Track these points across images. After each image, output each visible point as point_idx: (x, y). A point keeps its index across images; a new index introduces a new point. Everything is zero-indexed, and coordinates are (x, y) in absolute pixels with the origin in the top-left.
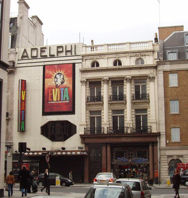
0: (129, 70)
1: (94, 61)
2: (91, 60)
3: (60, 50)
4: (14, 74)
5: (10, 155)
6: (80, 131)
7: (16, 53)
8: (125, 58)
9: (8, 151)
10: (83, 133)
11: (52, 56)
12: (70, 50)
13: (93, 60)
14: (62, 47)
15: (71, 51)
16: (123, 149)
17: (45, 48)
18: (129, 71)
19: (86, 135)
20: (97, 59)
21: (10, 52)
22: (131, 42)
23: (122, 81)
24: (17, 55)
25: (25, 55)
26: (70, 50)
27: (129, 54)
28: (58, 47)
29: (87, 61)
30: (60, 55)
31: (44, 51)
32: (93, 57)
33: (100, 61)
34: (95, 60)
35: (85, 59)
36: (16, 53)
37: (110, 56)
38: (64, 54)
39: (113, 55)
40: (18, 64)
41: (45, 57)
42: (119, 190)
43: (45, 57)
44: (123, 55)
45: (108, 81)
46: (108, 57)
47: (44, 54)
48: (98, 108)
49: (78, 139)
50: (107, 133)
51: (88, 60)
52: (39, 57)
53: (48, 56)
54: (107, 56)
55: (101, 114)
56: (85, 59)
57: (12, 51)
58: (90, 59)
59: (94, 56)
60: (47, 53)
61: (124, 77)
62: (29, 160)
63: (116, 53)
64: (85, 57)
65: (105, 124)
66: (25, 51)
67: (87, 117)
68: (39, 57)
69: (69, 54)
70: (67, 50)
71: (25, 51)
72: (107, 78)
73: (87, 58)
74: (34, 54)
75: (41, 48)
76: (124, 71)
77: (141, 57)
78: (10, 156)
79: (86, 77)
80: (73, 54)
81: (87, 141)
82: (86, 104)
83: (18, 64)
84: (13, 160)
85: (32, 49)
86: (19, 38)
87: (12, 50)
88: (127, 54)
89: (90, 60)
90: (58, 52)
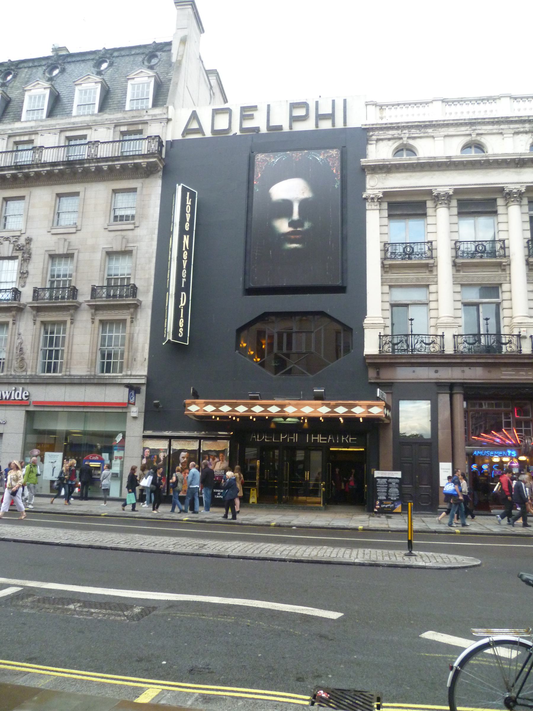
0: (517, 167)
1: (403, 143)
2: (394, 141)
3: (300, 112)
5: (135, 415)
7: (169, 120)
8: (499, 137)
9: (132, 401)
12: (330, 112)
13: (401, 142)
14: (304, 105)
16: (497, 405)
17: (255, 108)
18: (518, 170)
19: (386, 357)
20: (414, 138)
21: (150, 118)
22: (515, 93)
23: (423, 205)
24: (171, 124)
26: (330, 112)
27: (512, 126)
28: (294, 106)
29: (381, 144)
31: (251, 117)
32: (399, 132)
33: (485, 140)
34: (405, 140)
35: (374, 137)
36: (169, 120)
37: (452, 131)
39: (463, 128)
42: (243, 520)
44: (490, 127)
45: (380, 200)
46: (446, 133)
48: (418, 278)
49: (489, 372)
50: (455, 350)
51: (385, 142)
54: (444, 131)
55: (498, 297)
56: (374, 137)
57: (155, 115)
58: (389, 139)
59: (404, 132)
61: (430, 192)
62: (199, 430)
63: (472, 123)
64: (376, 133)
65: (374, 326)
66: (194, 116)
67: (509, 306)
70: (321, 112)
71: (194, 116)
72: (446, 189)
73: (381, 134)
75: (243, 109)
76: (501, 170)
77: (411, 142)
78: (135, 418)
79: (380, 185)
82: (383, 266)
84: (145, 428)
85: (216, 112)
86: (177, 84)
87: (157, 111)
88: (502, 127)
89: (391, 143)
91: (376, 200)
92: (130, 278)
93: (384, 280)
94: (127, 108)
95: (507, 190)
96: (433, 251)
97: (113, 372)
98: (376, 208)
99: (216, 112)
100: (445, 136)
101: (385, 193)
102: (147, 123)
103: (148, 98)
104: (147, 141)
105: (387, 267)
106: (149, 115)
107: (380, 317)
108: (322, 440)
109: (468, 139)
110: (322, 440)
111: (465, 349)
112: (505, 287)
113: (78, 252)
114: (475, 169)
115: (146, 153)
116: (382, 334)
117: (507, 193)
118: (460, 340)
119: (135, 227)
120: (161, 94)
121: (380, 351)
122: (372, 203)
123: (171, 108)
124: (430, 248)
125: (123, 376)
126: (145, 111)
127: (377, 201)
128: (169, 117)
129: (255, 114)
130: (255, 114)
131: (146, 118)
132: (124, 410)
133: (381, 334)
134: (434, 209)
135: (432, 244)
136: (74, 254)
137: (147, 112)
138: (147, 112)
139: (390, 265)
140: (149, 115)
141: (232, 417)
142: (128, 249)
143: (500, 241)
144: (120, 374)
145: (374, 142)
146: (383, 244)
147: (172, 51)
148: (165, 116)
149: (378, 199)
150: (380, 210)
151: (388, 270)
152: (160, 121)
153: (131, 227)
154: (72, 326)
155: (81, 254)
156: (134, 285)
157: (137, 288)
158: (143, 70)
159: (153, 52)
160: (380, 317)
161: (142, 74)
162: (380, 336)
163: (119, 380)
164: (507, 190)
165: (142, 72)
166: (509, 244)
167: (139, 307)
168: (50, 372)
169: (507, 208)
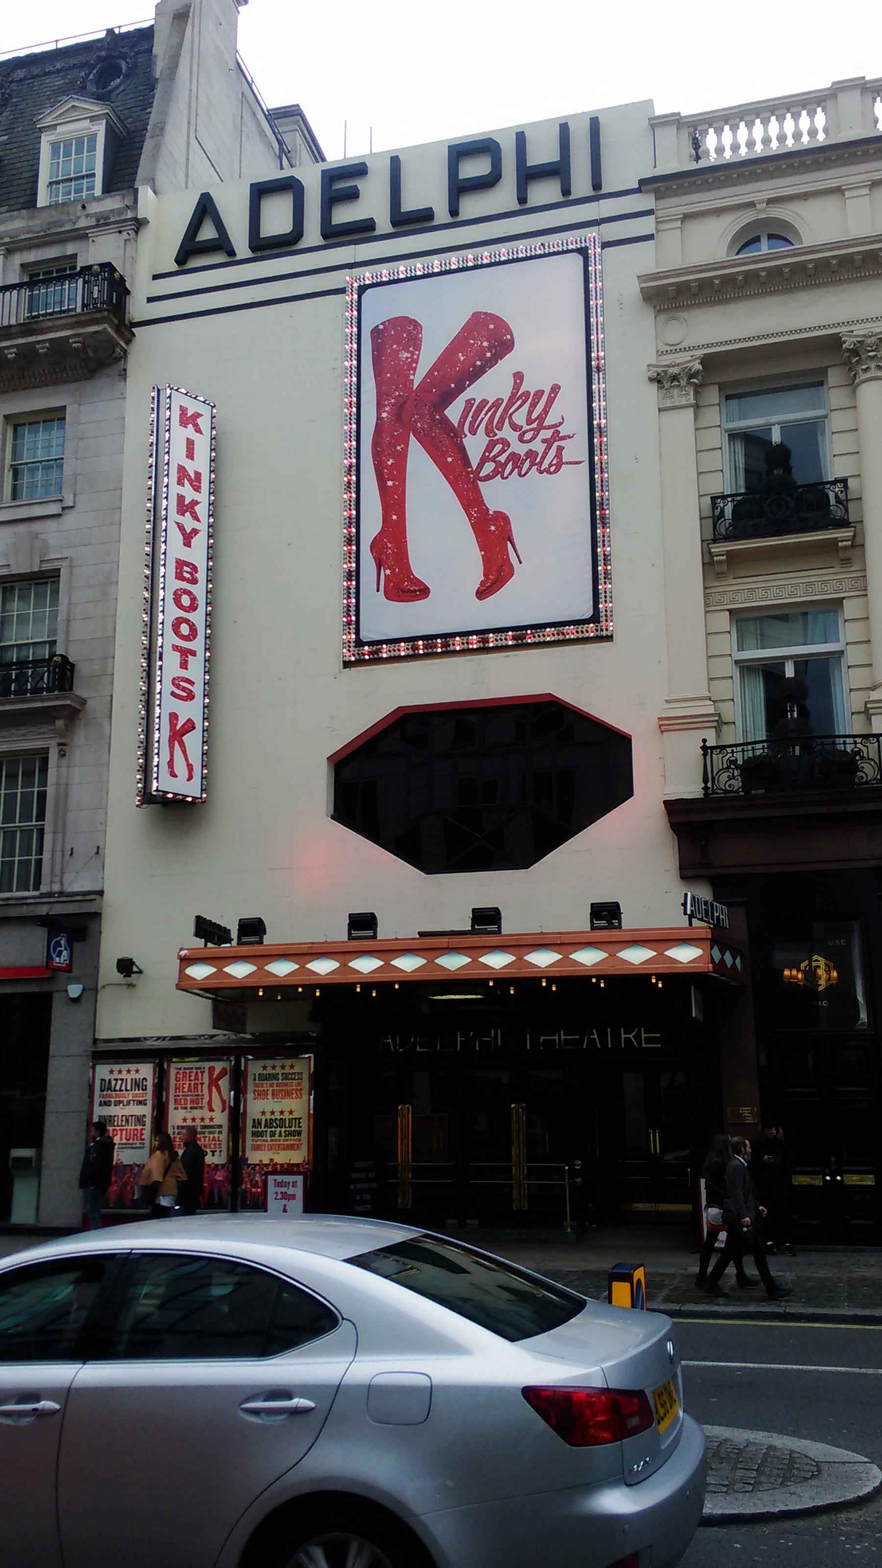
3: (475, 168)
4: (123, 375)
6: (666, 770)
7: (139, 224)
10: (690, 788)
11: (422, 220)
14: (485, 147)
15: (558, 171)
24: (147, 236)
25: (207, 233)
28: (460, 152)
30: (472, 206)
31: (353, 195)
38: (504, 196)
40: (150, 300)
41: (363, 230)
43: (363, 230)
46: (773, 194)
47: (343, 215)
52: (312, 235)
53: (384, 225)
60: (372, 204)
66: (206, 208)
68: (312, 235)
69: (544, 192)
71: (206, 208)
74: (277, 218)
80: (581, 185)
81: (737, 854)
83: (150, 300)
86: (162, 129)
87: (113, 203)
90: (459, 189)
91: (683, 383)
92: (55, 641)
93: (860, 583)
94: (42, 200)
95: (849, 343)
96: (851, 505)
97: (17, 891)
98: (684, 402)
99: (260, 192)
100: (687, 217)
101: (706, 361)
102: (85, 237)
103: (93, 175)
104: (81, 281)
105: (720, 562)
106: (87, 216)
107: (704, 698)
108: (648, 1041)
109: (748, 217)
110: (648, 1041)
111: (732, 782)
112: (851, 608)
113: (71, 567)
114: (817, 286)
115: (22, 321)
116: (711, 743)
117: (854, 352)
118: (717, 759)
119: (63, 508)
120: (124, 161)
121: (705, 789)
122: (676, 392)
123: (145, 194)
124: (842, 496)
125: (42, 896)
126: (79, 207)
127: (689, 383)
128: (140, 216)
129: (361, 184)
130: (361, 184)
131: (83, 223)
132: (46, 988)
133: (707, 744)
134: (849, 389)
135: (846, 487)
136: (59, 570)
137: (84, 207)
138: (84, 207)
139: (729, 554)
140: (87, 216)
141: (598, 982)
142: (46, 567)
143: (834, 482)
144: (36, 893)
145: (679, 224)
146: (708, 501)
147: (155, 50)
148: (130, 215)
149: (691, 376)
150: (697, 407)
151: (724, 568)
152: (120, 226)
153: (54, 509)
154: (64, 761)
155: (76, 571)
156: (65, 658)
157: (73, 666)
158: (76, 104)
159: (109, 57)
160: (704, 698)
161: (76, 115)
162: (704, 748)
163: (31, 908)
164: (849, 343)
165: (73, 106)
166: (861, 488)
167: (81, 715)
168: (12, 891)
169: (854, 392)
